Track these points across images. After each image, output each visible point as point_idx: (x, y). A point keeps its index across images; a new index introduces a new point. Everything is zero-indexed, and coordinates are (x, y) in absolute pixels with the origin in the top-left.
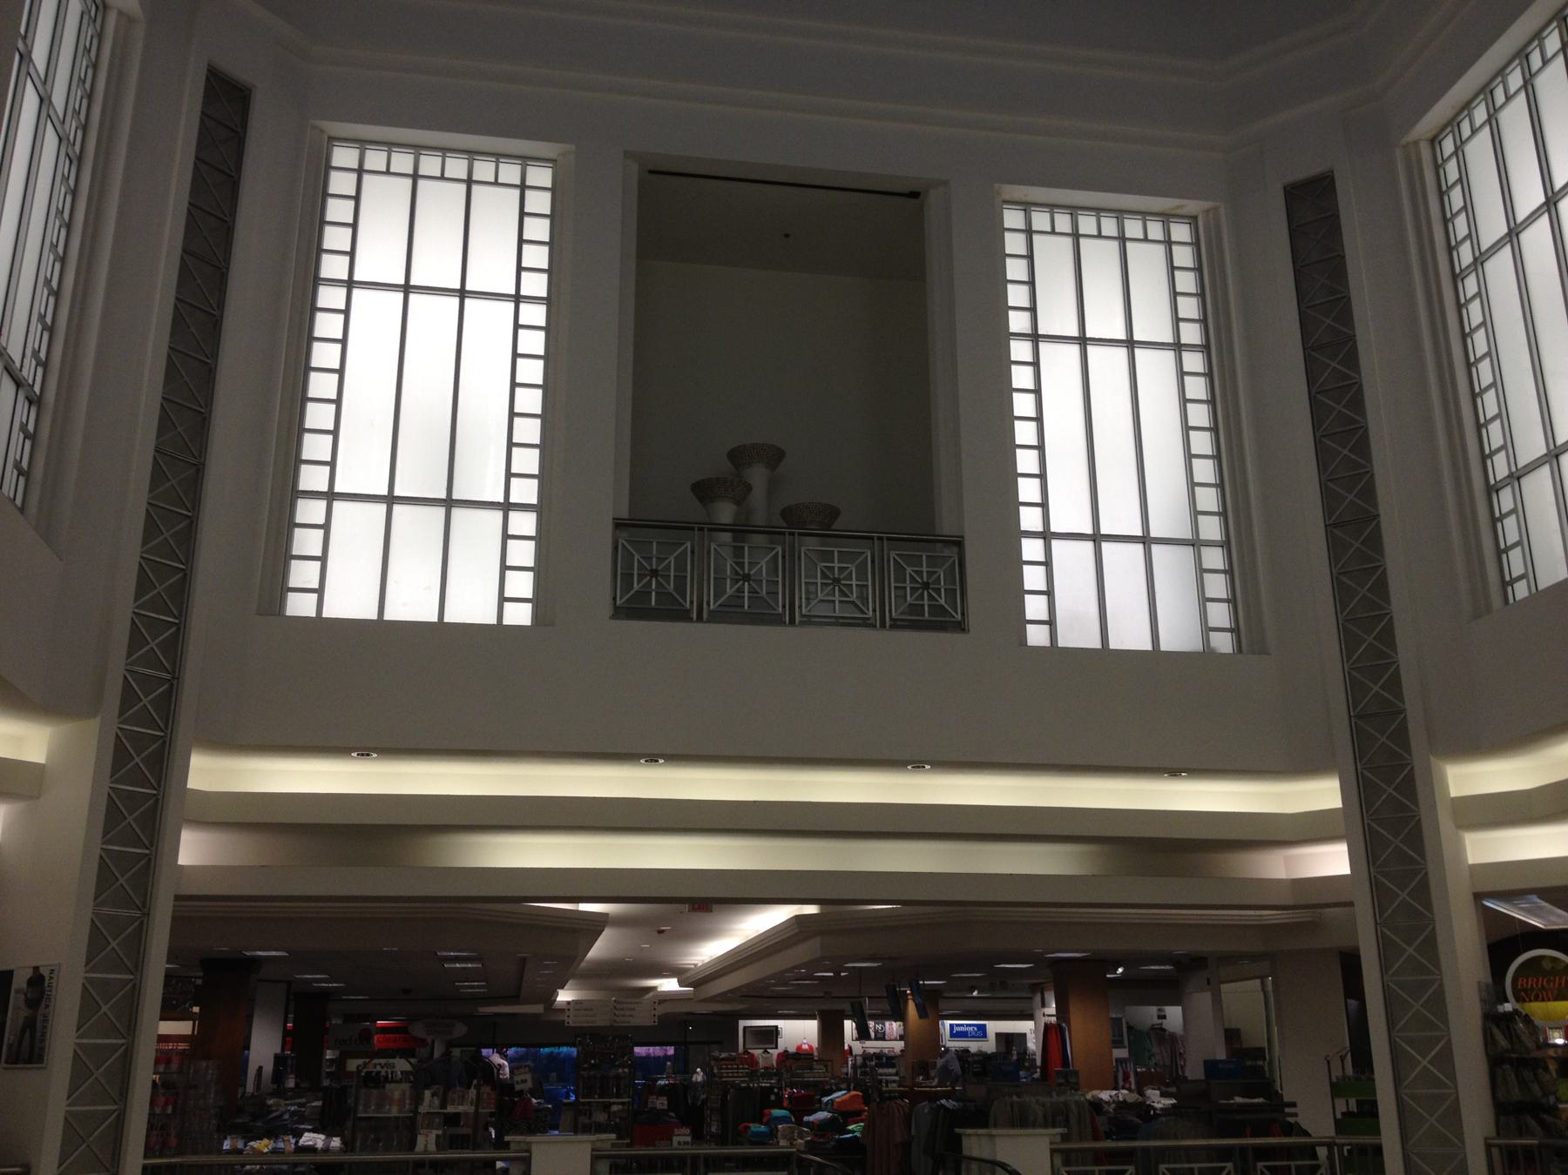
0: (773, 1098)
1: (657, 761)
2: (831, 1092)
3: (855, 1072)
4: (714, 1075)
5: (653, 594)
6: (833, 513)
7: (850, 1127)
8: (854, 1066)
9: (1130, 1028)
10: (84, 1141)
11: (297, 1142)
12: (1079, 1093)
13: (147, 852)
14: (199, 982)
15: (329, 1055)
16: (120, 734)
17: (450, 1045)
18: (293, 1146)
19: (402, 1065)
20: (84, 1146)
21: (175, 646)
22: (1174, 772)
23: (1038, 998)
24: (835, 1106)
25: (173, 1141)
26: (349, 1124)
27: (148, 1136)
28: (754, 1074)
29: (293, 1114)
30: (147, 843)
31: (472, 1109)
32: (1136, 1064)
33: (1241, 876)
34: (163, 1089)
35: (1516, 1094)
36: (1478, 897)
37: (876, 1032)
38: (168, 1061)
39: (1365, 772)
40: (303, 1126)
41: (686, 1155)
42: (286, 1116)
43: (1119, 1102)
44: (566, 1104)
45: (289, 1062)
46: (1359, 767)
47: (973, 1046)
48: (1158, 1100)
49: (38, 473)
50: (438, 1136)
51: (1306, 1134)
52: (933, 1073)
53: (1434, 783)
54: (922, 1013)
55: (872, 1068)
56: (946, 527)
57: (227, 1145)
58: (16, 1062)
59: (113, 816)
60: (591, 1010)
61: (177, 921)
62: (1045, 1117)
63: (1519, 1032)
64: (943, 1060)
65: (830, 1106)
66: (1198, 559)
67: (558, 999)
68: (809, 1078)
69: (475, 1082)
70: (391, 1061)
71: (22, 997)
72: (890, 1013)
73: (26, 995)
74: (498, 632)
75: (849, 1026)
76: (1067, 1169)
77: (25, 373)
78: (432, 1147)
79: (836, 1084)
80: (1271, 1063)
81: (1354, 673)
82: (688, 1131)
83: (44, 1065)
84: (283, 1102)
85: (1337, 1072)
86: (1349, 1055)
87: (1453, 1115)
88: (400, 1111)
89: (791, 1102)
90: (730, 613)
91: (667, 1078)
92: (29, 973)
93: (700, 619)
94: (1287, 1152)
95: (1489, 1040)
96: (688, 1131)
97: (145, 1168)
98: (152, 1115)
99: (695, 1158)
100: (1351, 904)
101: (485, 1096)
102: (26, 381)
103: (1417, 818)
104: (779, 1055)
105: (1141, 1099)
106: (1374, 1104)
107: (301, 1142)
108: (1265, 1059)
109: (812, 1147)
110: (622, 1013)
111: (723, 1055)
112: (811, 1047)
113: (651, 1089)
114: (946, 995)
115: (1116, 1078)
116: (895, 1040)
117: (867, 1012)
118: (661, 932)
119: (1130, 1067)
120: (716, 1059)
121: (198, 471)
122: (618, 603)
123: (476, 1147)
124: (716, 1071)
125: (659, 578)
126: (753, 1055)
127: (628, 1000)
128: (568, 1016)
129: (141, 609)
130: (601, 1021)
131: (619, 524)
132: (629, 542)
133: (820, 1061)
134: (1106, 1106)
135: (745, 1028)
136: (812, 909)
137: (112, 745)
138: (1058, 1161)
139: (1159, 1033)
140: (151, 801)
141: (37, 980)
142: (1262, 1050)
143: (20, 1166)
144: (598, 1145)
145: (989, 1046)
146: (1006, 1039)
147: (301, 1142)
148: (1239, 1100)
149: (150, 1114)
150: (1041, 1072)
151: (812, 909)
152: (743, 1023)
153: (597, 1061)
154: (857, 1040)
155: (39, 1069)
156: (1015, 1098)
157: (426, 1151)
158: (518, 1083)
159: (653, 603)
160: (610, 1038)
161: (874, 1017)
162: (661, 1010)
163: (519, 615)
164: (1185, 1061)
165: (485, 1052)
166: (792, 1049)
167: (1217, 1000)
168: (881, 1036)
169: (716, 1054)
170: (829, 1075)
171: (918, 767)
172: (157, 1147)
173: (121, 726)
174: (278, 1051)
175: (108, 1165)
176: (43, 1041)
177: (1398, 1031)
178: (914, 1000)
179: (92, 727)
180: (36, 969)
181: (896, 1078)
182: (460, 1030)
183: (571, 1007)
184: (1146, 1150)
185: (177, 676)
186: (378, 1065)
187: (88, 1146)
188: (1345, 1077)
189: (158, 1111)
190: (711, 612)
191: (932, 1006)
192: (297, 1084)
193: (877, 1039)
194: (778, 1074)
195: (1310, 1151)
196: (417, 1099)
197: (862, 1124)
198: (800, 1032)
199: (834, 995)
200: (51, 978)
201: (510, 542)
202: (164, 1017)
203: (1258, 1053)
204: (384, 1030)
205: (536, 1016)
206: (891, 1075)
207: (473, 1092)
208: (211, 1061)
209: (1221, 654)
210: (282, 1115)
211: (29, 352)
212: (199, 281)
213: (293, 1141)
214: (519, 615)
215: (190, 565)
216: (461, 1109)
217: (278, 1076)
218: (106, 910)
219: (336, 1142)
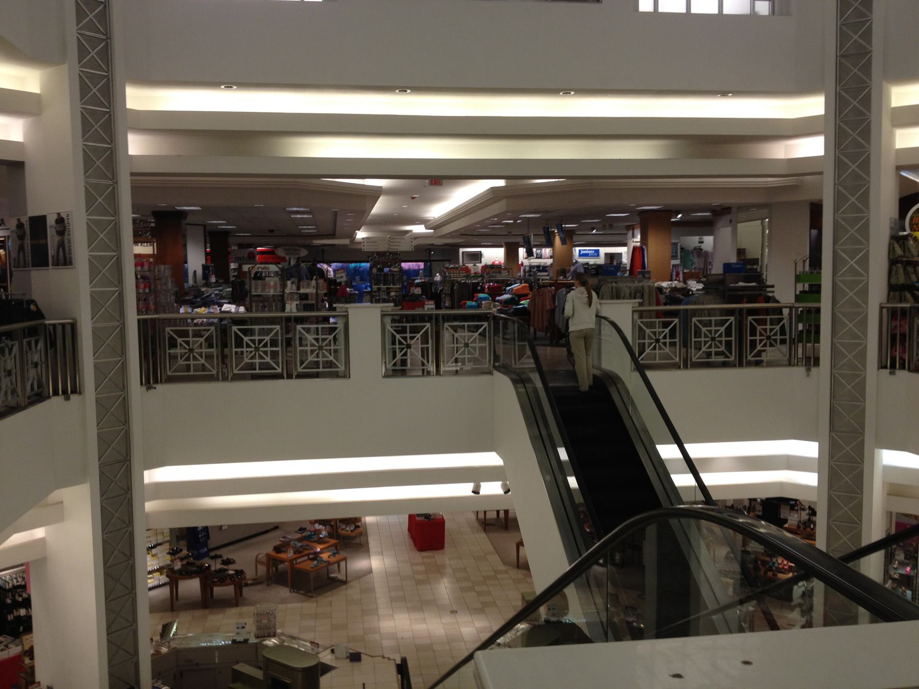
0: (479, 288)
2: (511, 285)
3: (525, 275)
4: (446, 277)
7: (522, 302)
8: (524, 271)
9: (682, 249)
10: (103, 307)
11: (220, 309)
12: (651, 281)
13: (110, 146)
14: (153, 225)
15: (233, 266)
16: (81, 74)
17: (298, 259)
18: (219, 311)
19: (273, 268)
20: (103, 309)
22: (724, 94)
23: (630, 233)
24: (514, 292)
25: (152, 307)
26: (248, 299)
27: (138, 305)
28: (468, 276)
29: (216, 295)
30: (109, 141)
31: (314, 291)
32: (684, 267)
33: (759, 158)
34: (142, 279)
35: (902, 280)
36: (899, 168)
37: (537, 254)
38: (142, 265)
39: (842, 92)
40: (222, 301)
41: (432, 314)
42: (213, 296)
43: (672, 288)
44: (366, 292)
45: (211, 268)
46: (837, 152)
47: (592, 261)
48: (695, 286)
50: (297, 305)
51: (778, 302)
52: (568, 275)
53: (883, 97)
54: (563, 242)
55: (535, 273)
57: (182, 310)
58: (58, 265)
61: (136, 189)
62: (630, 294)
63: (909, 246)
64: (574, 267)
65: (510, 292)
67: (357, 237)
68: (499, 277)
69: (314, 277)
70: (267, 266)
71: (54, 230)
72: (545, 244)
73: (56, 228)
75: (522, 252)
76: (641, 320)
78: (294, 310)
79: (514, 281)
80: (761, 267)
81: (844, 28)
82: (433, 302)
84: (210, 290)
85: (800, 269)
86: (808, 260)
87: (864, 293)
88: (275, 292)
89: (489, 290)
91: (421, 279)
92: (55, 217)
94: (766, 311)
95: (891, 250)
96: (433, 302)
97: (139, 320)
98: (138, 293)
99: (437, 316)
100: (821, 173)
101: (321, 285)
103: (869, 120)
104: (482, 267)
105: (685, 286)
106: (819, 286)
107: (223, 309)
108: (758, 265)
109: (500, 311)
110: (394, 244)
111: (451, 266)
112: (500, 262)
113: (412, 284)
114: (577, 233)
115: (672, 275)
116: (548, 258)
117: (532, 243)
118: (413, 198)
119: (680, 270)
120: (447, 268)
123: (319, 310)
124: (447, 274)
126: (467, 267)
129: (88, 141)
130: (382, 248)
133: (505, 269)
134: (665, 291)
135: (463, 252)
136: (501, 183)
137: (83, 193)
138: (636, 316)
139: (699, 251)
140: (107, 116)
141: (60, 220)
142: (757, 260)
143: (72, 319)
144: (384, 309)
145: (601, 260)
146: (611, 257)
147: (223, 309)
148: (741, 284)
149: (137, 293)
150: (629, 273)
151: (501, 183)
152: (461, 250)
154: (526, 258)
155: (70, 268)
156: (614, 284)
157: (291, 312)
158: (338, 278)
160: (387, 254)
161: (536, 246)
162: (416, 243)
164: (712, 266)
165: (319, 266)
166: (490, 263)
167: (735, 232)
168: (539, 257)
169: (447, 265)
170: (510, 276)
171: (567, 93)
172: (144, 310)
173: (81, 69)
174: (204, 263)
175: (118, 319)
176: (70, 253)
177: (839, 245)
178: (559, 235)
179: (64, 68)
181: (548, 278)
182: (304, 253)
184: (687, 310)
186: (259, 267)
187: (106, 309)
188: (804, 272)
189: (141, 291)
191: (569, 238)
192: (217, 281)
193: (537, 258)
194: (482, 276)
195: (779, 311)
196: (284, 286)
197: (528, 300)
198: (494, 255)
199: (513, 233)
200: (68, 219)
202: (136, 242)
203: (755, 261)
204: (261, 252)
205: (345, 246)
206: (545, 276)
207: (314, 283)
208: (166, 266)
209: (762, 16)
210: (210, 295)
213: (219, 308)
215: (126, 390)
216: (308, 291)
217: (206, 276)
218: (93, 181)
219: (242, 309)
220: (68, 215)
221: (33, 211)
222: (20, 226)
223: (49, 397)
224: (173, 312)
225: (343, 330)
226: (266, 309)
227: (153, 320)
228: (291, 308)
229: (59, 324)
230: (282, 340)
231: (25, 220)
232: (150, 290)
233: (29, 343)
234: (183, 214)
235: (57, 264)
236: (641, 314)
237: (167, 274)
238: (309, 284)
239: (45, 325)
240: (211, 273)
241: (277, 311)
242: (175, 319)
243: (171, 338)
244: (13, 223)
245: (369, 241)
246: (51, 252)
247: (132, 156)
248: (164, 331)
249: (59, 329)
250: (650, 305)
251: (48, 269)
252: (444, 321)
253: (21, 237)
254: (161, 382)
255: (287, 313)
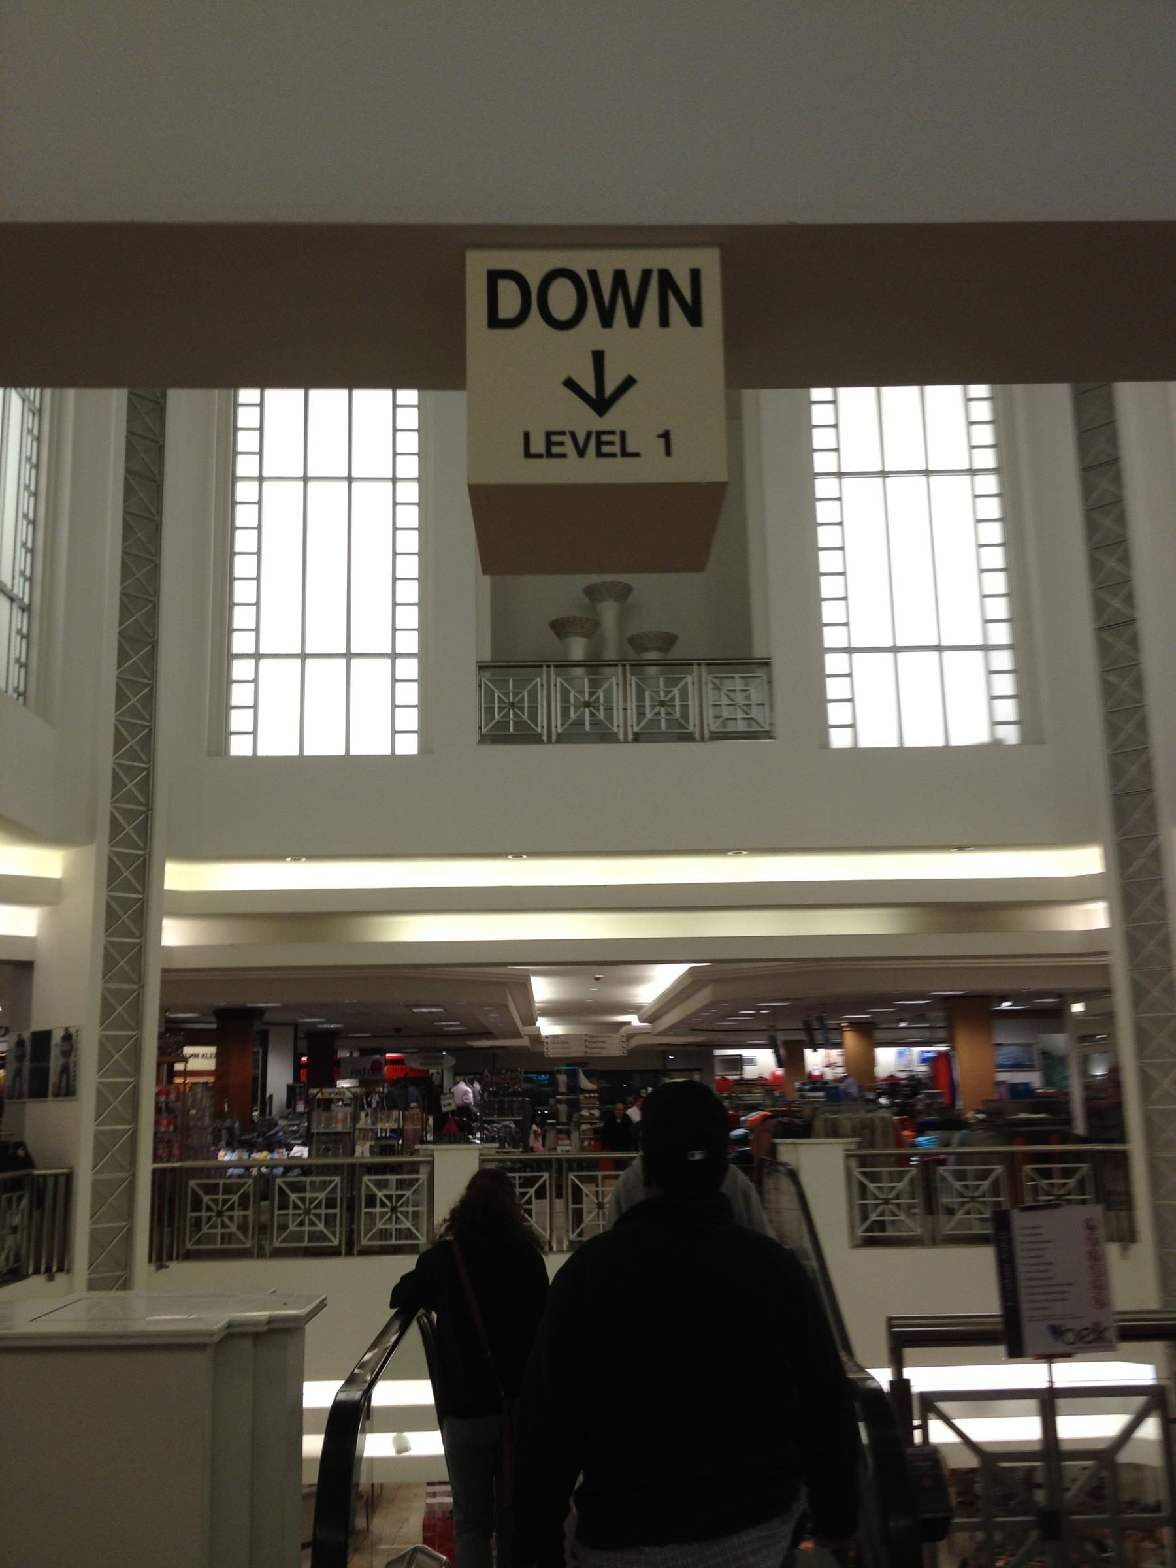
1: (521, 857)
5: (511, 722)
6: (668, 641)
11: (289, 1154)
21: (147, 785)
33: (1047, 930)
49: (33, 663)
50: (371, 1146)
56: (759, 652)
59: (111, 917)
60: (567, 1043)
66: (987, 662)
74: (392, 761)
77: (15, 591)
78: (367, 1153)
83: (76, 1097)
88: (343, 1128)
90: (572, 735)
92: (61, 1033)
93: (550, 741)
102: (17, 596)
118: (597, 979)
121: (153, 648)
122: (483, 731)
125: (516, 709)
127: (602, 1034)
128: (547, 1049)
130: (577, 1052)
131: (482, 667)
132: (491, 681)
141: (68, 1037)
144: (485, 1152)
153: (495, 1089)
157: (362, 1157)
158: (444, 1106)
159: (511, 729)
160: (504, 1071)
162: (634, 1043)
163: (409, 746)
171: (738, 853)
174: (290, 1081)
176: (75, 1080)
180: (67, 1029)
183: (549, 1041)
185: (150, 807)
190: (559, 735)
191: (871, 1034)
196: (355, 1119)
201: (398, 684)
211: (17, 573)
212: (141, 494)
213: (287, 1153)
214: (409, 746)
220: (77, 1031)
221: (38, 1025)
222: (20, 1043)
223: (26, 1276)
224: (208, 1159)
225: (425, 1183)
226: (330, 1153)
227: (173, 1169)
228: (363, 1151)
229: (51, 1175)
230: (341, 1199)
231: (26, 1036)
232: (176, 1127)
233: (10, 1200)
234: (257, 1013)
235: (57, 1094)
236: (863, 1161)
237: (204, 1105)
238: (389, 1116)
239: (33, 1177)
240: (298, 1097)
241: (345, 1154)
242: (209, 1169)
243: (195, 1194)
244: (13, 1037)
245: (555, 1040)
246: (53, 1078)
247: (170, 949)
248: (187, 1184)
249: (51, 1181)
250: (886, 1146)
251: (45, 1101)
252: (570, 1169)
253: (20, 1058)
254: (177, 1258)
255: (357, 1158)
